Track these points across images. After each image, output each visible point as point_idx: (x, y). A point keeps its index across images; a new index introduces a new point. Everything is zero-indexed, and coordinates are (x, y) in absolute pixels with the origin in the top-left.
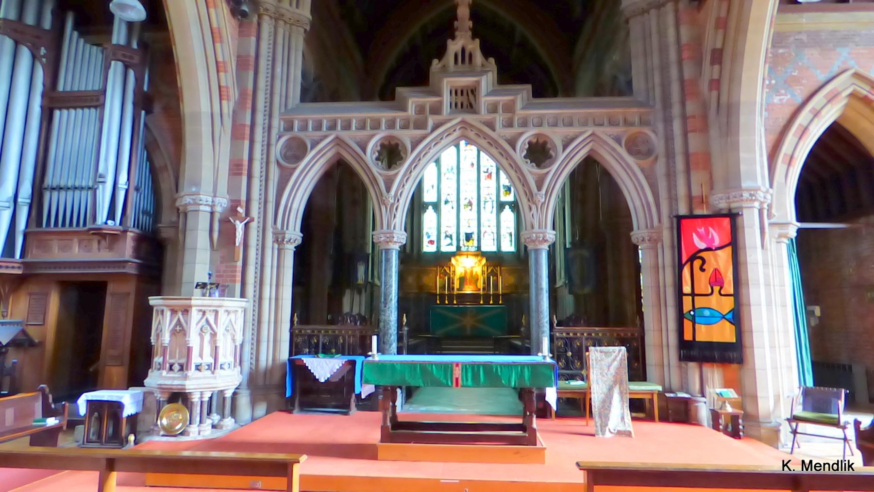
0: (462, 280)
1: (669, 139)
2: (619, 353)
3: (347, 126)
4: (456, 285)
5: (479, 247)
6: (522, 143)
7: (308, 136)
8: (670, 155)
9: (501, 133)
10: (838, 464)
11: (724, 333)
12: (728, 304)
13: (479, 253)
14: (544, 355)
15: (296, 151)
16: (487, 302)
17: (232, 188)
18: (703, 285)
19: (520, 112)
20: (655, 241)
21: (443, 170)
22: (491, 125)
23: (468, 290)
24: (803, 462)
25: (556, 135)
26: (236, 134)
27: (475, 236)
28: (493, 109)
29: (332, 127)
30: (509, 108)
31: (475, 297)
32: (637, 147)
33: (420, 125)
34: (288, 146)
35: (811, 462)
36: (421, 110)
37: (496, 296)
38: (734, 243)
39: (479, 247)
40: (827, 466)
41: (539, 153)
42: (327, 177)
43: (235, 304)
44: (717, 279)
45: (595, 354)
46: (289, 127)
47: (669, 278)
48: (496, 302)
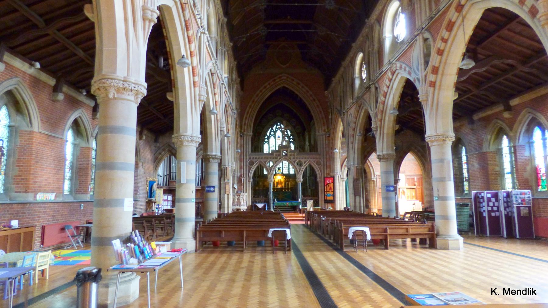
0: (278, 183)
1: (324, 162)
2: (312, 201)
3: (262, 158)
4: (276, 185)
5: (282, 172)
6: (296, 162)
7: (254, 160)
8: (324, 165)
9: (292, 160)
10: (526, 291)
11: (332, 198)
12: (332, 193)
13: (282, 174)
14: (300, 200)
15: (252, 164)
16: (285, 190)
17: (240, 171)
18: (328, 190)
19: (296, 156)
20: (321, 181)
21: (270, 146)
22: (290, 158)
23: (279, 186)
24: (504, 289)
25: (303, 161)
26: (241, 161)
27: (281, 169)
28: (291, 155)
29: (259, 158)
30: (294, 155)
31: (281, 189)
32: (318, 163)
33: (276, 158)
34: (250, 162)
35: (509, 289)
36: (276, 155)
37: (288, 188)
38: (334, 182)
39: (282, 172)
40: (519, 292)
41: (300, 164)
42: (258, 167)
43: (246, 194)
44: (331, 189)
45: (308, 202)
46: (250, 158)
47: (323, 188)
48: (288, 190)
